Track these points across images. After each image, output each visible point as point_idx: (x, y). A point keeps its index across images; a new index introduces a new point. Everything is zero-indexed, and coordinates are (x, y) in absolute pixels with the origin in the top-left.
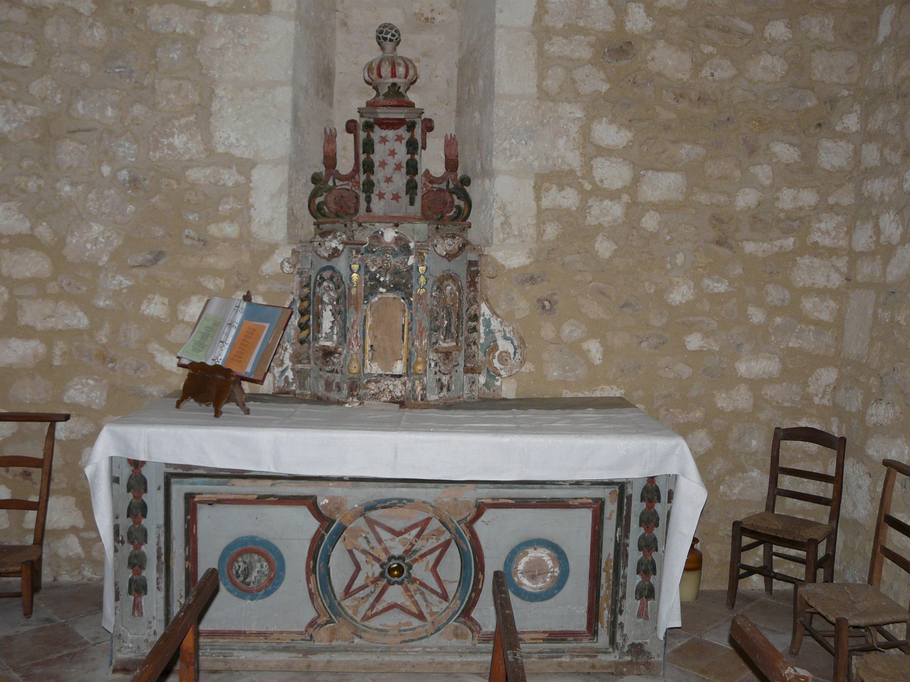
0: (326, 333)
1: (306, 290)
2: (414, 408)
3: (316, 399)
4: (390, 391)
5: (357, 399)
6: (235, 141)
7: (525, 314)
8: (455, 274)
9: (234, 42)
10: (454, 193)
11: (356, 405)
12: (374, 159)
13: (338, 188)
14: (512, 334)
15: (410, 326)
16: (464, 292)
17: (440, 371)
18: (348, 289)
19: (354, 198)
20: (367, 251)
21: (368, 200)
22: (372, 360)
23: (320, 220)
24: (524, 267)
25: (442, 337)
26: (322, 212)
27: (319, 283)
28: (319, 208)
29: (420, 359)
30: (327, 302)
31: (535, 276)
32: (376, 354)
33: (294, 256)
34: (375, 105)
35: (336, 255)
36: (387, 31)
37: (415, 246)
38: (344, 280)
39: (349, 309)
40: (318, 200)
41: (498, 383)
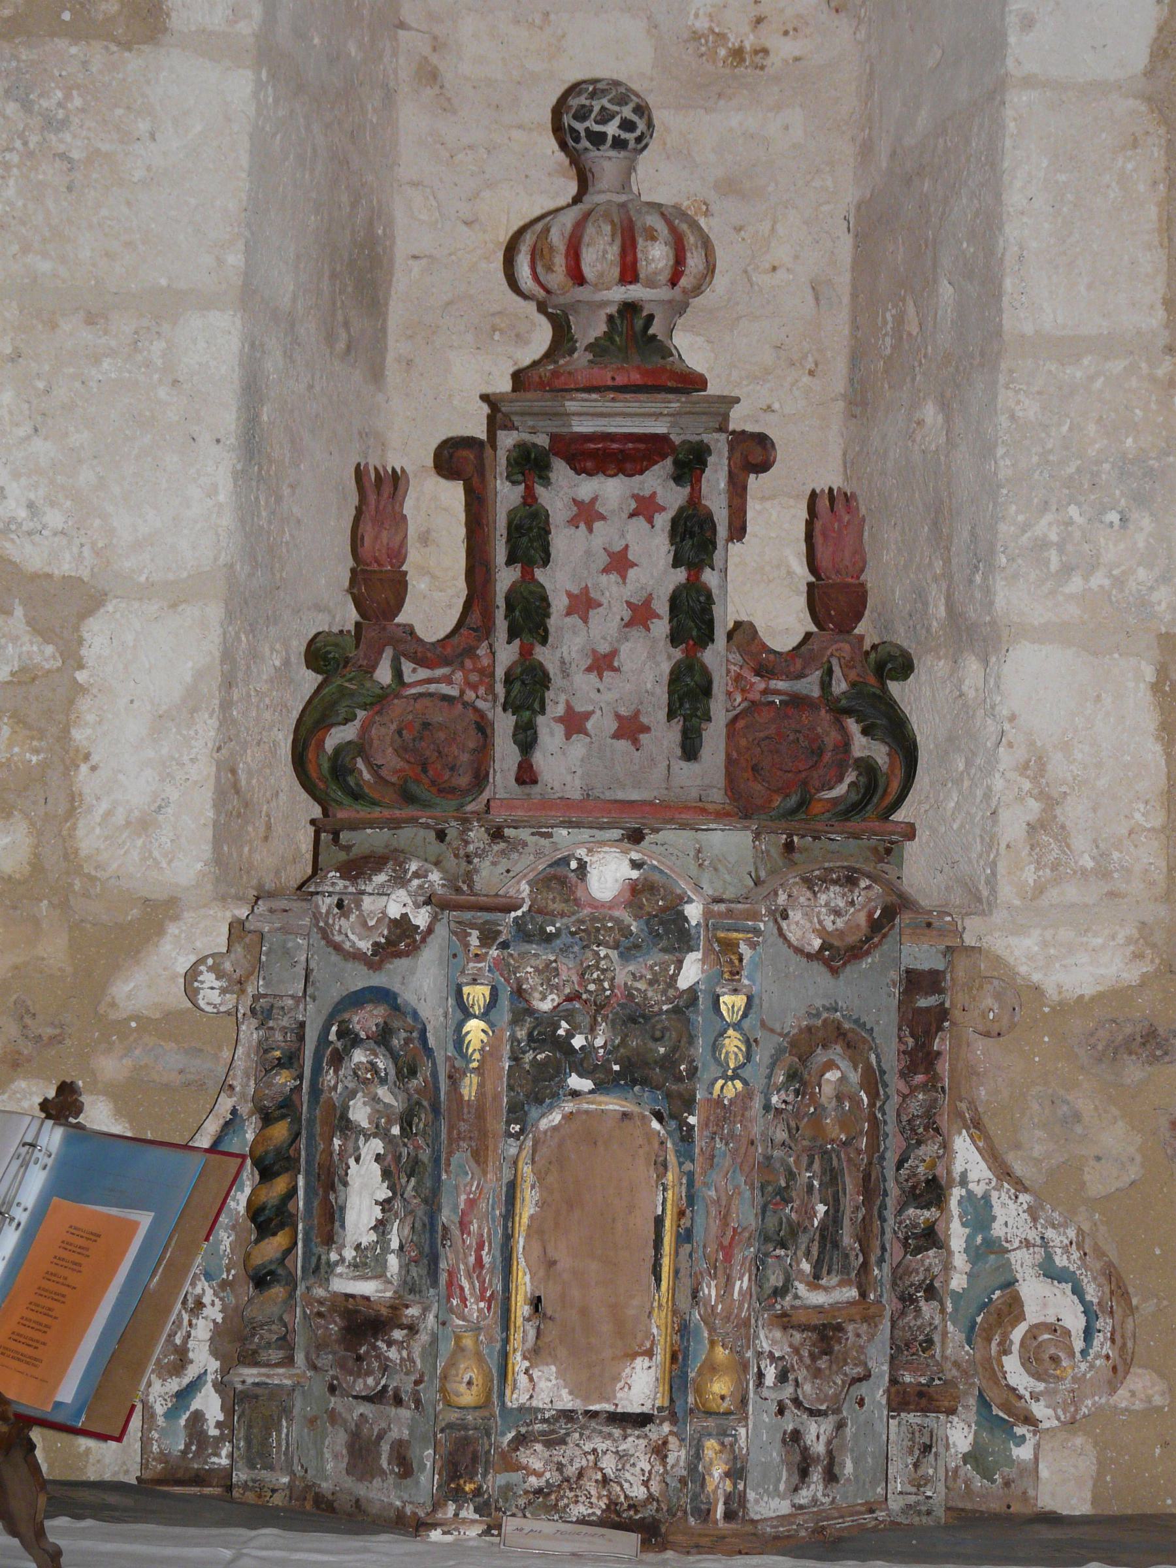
0: (358, 1247)
1: (283, 1080)
2: (699, 1549)
3: (309, 1505)
4: (605, 1481)
5: (476, 1511)
6: (22, 513)
7: (1127, 1179)
8: (857, 1021)
9: (25, 144)
10: (848, 712)
11: (473, 1532)
12: (548, 586)
13: (413, 691)
14: (1076, 1255)
15: (687, 1223)
16: (891, 1091)
17: (797, 1402)
18: (450, 1077)
19: (473, 732)
20: (523, 932)
21: (526, 739)
22: (535, 1354)
23: (341, 814)
24: (1117, 996)
25: (806, 1267)
26: (351, 781)
27: (336, 1050)
28: (340, 768)
29: (721, 1353)
30: (365, 1124)
31: (1161, 1031)
32: (552, 1332)
33: (239, 949)
34: (558, 383)
35: (402, 946)
36: (603, 108)
37: (707, 914)
38: (432, 1042)
39: (450, 1153)
40: (339, 736)
41: (1023, 1453)
